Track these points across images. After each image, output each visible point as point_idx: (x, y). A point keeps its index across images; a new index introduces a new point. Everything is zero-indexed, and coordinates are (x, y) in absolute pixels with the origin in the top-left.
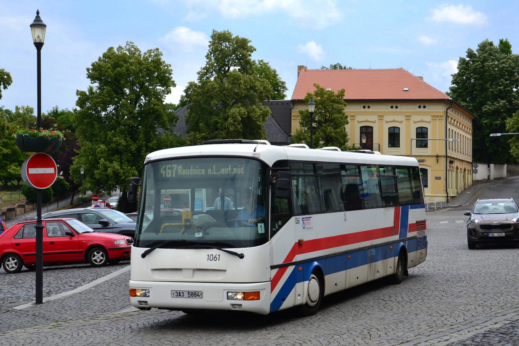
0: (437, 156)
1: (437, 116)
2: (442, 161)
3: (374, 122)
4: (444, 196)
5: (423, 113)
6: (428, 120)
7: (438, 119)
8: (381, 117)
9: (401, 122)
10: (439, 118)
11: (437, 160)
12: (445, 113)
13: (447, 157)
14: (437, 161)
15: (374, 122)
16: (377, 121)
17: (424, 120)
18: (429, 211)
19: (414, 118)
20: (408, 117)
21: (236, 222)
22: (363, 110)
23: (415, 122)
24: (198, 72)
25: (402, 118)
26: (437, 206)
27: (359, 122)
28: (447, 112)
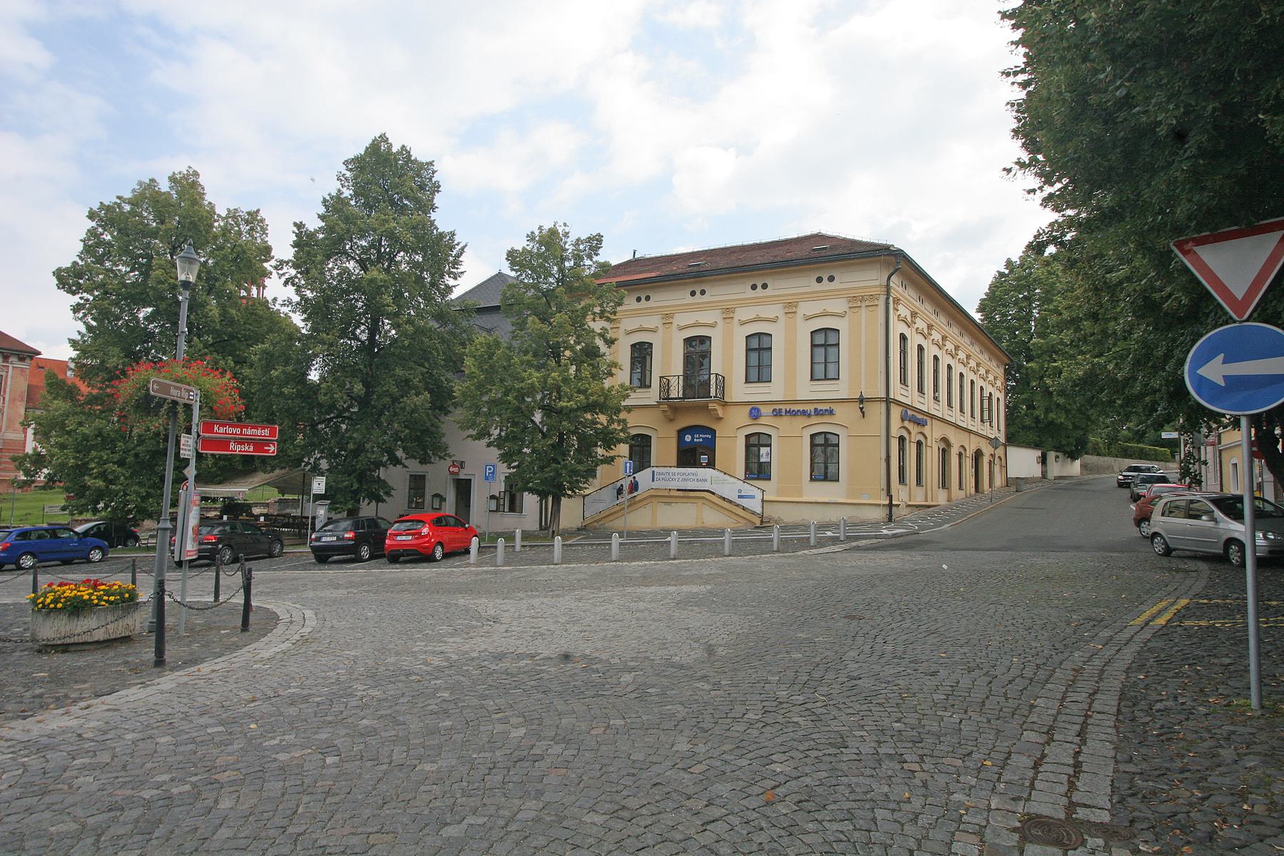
0: (861, 400)
1: (863, 299)
2: (877, 411)
3: (713, 326)
4: (879, 505)
5: (814, 295)
6: (840, 311)
7: (864, 304)
8: (728, 312)
9: (774, 320)
11: (861, 409)
12: (885, 289)
13: (888, 401)
15: (713, 326)
16: (720, 322)
17: (830, 310)
18: (778, 551)
20: (790, 307)
21: (1200, 372)
22: (752, 294)
23: (808, 318)
25: (774, 310)
26: (815, 534)
27: (682, 329)
28: (888, 287)
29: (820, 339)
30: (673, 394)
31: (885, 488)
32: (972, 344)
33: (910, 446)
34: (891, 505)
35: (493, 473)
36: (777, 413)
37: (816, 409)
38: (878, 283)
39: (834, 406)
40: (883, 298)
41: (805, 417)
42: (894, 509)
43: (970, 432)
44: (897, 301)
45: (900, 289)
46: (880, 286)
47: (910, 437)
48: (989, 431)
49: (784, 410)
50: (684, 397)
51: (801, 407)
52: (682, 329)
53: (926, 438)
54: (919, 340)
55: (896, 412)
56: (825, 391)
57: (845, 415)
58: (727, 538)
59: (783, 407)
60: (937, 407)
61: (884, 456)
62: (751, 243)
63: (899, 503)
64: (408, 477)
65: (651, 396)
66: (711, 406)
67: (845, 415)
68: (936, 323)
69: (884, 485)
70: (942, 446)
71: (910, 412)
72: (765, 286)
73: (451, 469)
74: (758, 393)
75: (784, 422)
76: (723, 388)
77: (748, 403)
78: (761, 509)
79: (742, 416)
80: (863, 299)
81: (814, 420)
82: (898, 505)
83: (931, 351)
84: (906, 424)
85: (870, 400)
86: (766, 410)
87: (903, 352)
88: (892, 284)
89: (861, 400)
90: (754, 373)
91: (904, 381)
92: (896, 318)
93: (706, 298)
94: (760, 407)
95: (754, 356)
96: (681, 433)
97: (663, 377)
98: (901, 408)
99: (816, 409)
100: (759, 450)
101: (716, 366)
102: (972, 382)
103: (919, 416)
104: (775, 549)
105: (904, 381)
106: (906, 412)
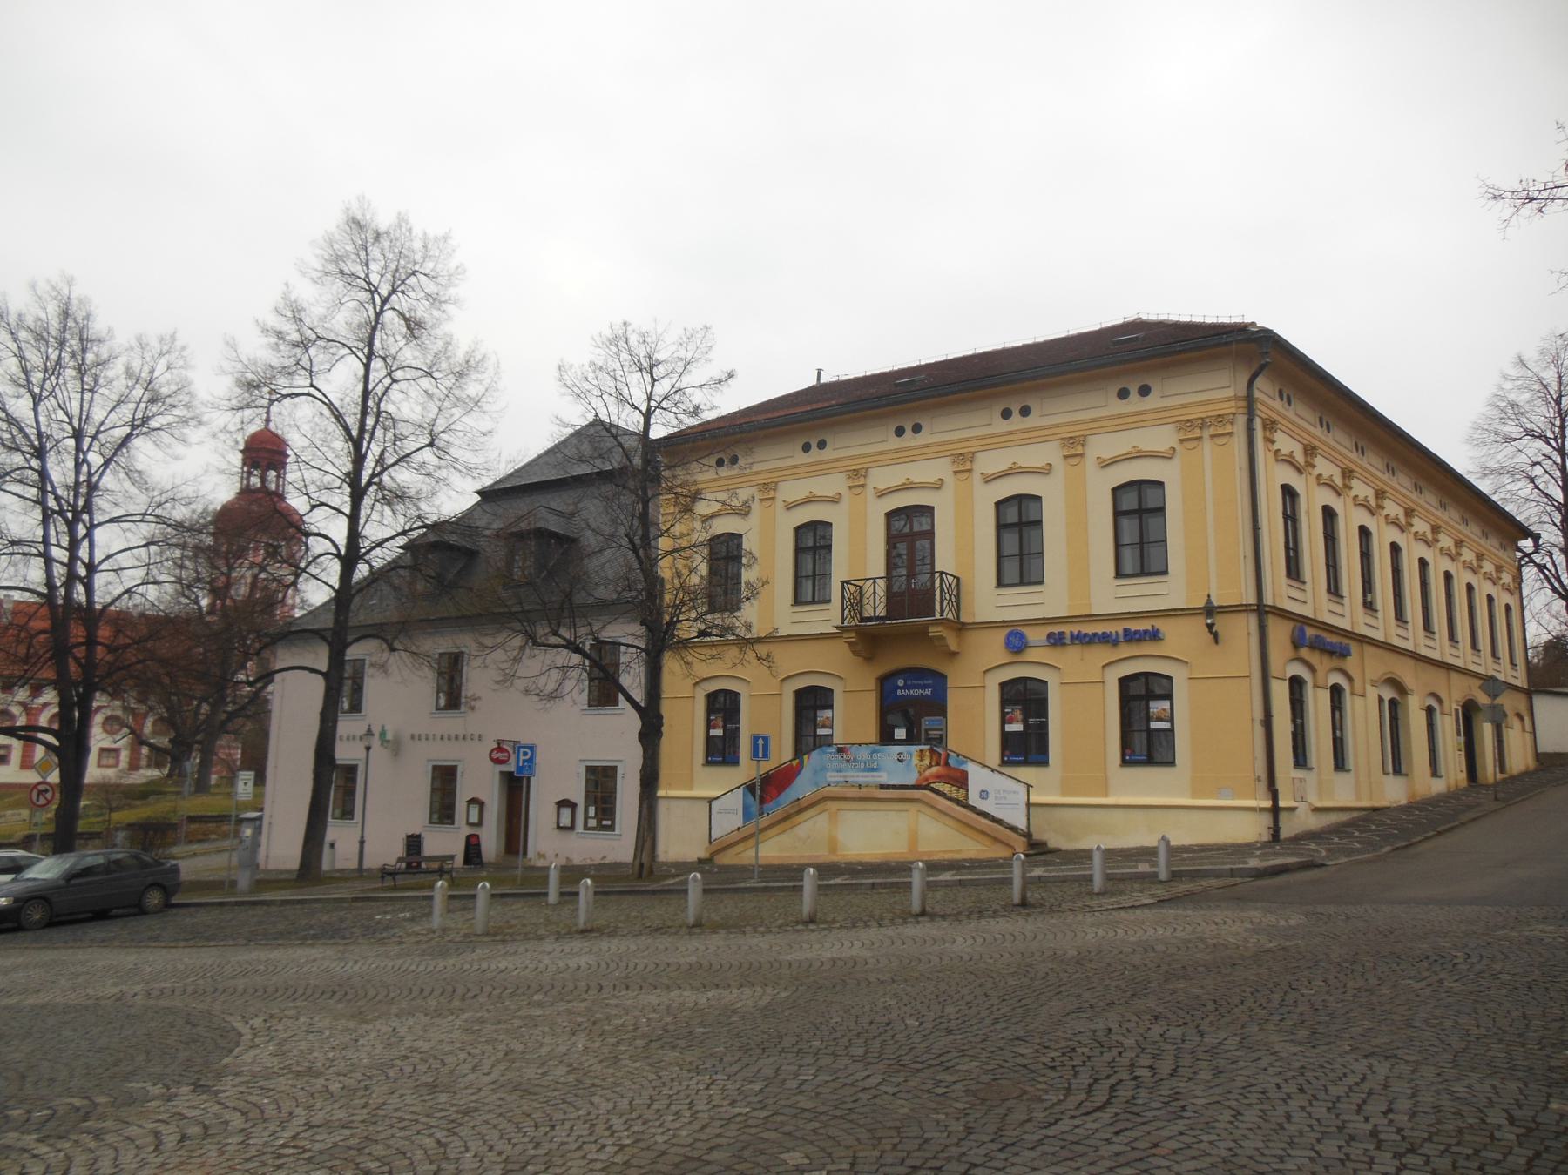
0: (1210, 610)
2: (1242, 631)
6: (1162, 447)
7: (1206, 434)
8: (963, 461)
9: (1045, 471)
10: (1212, 431)
11: (1210, 627)
12: (1244, 404)
13: (1262, 611)
14: (364, 751)
16: (949, 479)
17: (916, 479)
19: (1103, 446)
20: (1074, 447)
23: (1105, 464)
28: (1250, 401)
29: (1129, 502)
30: (868, 611)
31: (1264, 776)
32: (1485, 535)
33: (1353, 702)
34: (1275, 810)
35: (531, 760)
36: (1056, 641)
37: (1126, 630)
38: (1230, 393)
39: (1159, 624)
40: (1241, 420)
42: (1283, 816)
43: (1449, 667)
44: (1270, 426)
45: (1278, 404)
46: (1236, 398)
48: (1510, 672)
50: (888, 617)
51: (1099, 628)
52: (882, 494)
53: (1350, 678)
54: (1446, 564)
55: (1280, 633)
56: (1143, 595)
57: (1182, 638)
60: (1515, 674)
61: (1259, 714)
62: (1019, 344)
63: (1292, 804)
64: (583, 771)
65: (828, 617)
66: (934, 631)
67: (1182, 638)
68: (1505, 561)
69: (1261, 769)
70: (1388, 694)
71: (1310, 632)
73: (495, 755)
74: (1019, 604)
75: (1070, 658)
76: (958, 596)
77: (1004, 624)
78: (1024, 820)
79: (992, 648)
81: (1126, 650)
82: (1293, 809)
84: (1304, 652)
86: (1036, 635)
88: (1257, 394)
90: (1012, 569)
91: (1293, 569)
92: (1271, 456)
94: (1025, 630)
95: (1011, 539)
96: (885, 683)
97: (848, 582)
99: (1126, 630)
101: (945, 559)
102: (1490, 599)
103: (1333, 639)
104: (916, 907)
105: (1293, 569)
106: (1302, 632)
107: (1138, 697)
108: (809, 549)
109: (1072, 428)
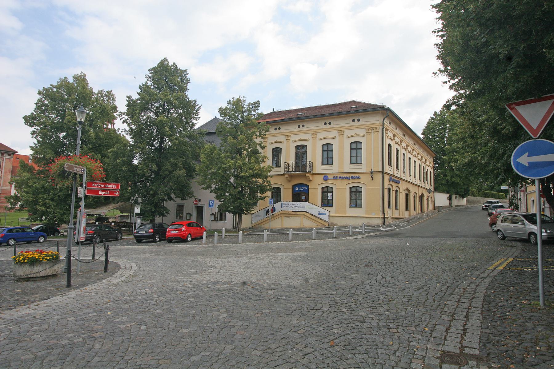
0: (372, 172)
1: (372, 129)
2: (378, 177)
3: (307, 140)
5: (351, 127)
6: (362, 134)
7: (373, 131)
8: (314, 135)
9: (334, 138)
11: (372, 176)
12: (382, 125)
13: (383, 173)
15: (307, 140)
16: (311, 139)
17: (358, 134)
18: (336, 238)
20: (341, 132)
21: (518, 160)
22: (324, 127)
23: (349, 137)
24: (26, 116)
25: (334, 134)
26: (352, 230)
27: (294, 142)
28: (383, 124)
29: (354, 146)
30: (291, 170)
31: (382, 210)
32: (419, 148)
33: (393, 192)
34: (384, 218)
35: (213, 204)
36: (335, 178)
37: (352, 176)
38: (379, 122)
39: (360, 175)
40: (381, 128)
41: (347, 180)
42: (386, 219)
43: (419, 186)
44: (387, 130)
45: (388, 125)
46: (380, 123)
47: (393, 189)
48: (427, 186)
49: (338, 177)
50: (295, 171)
51: (346, 176)
52: (294, 142)
53: (399, 189)
54: (397, 146)
55: (387, 178)
56: (356, 168)
57: (365, 179)
58: (313, 232)
59: (338, 176)
61: (381, 196)
62: (324, 105)
63: (388, 217)
64: (176, 206)
65: (281, 171)
66: (307, 175)
67: (365, 179)
68: (404, 139)
69: (381, 209)
70: (407, 192)
71: (393, 178)
72: (330, 123)
73: (195, 202)
74: (327, 169)
75: (338, 182)
76: (312, 167)
77: (323, 174)
78: (328, 219)
79: (320, 179)
80: (372, 129)
81: (351, 181)
82: (387, 218)
83: (402, 151)
84: (391, 183)
85: (375, 172)
86: (330, 177)
87: (390, 152)
88: (385, 122)
89: (372, 173)
90: (325, 161)
91: (390, 164)
92: (387, 137)
93: (304, 128)
94: (328, 175)
95: (325, 153)
96: (294, 187)
97: (286, 163)
98: (389, 176)
99: (352, 176)
100: (327, 194)
101: (309, 158)
102: (419, 165)
103: (397, 179)
104: (334, 237)
105: (390, 164)
106: (391, 178)
107: (326, 192)
108: (326, 151)
109: (369, 125)
